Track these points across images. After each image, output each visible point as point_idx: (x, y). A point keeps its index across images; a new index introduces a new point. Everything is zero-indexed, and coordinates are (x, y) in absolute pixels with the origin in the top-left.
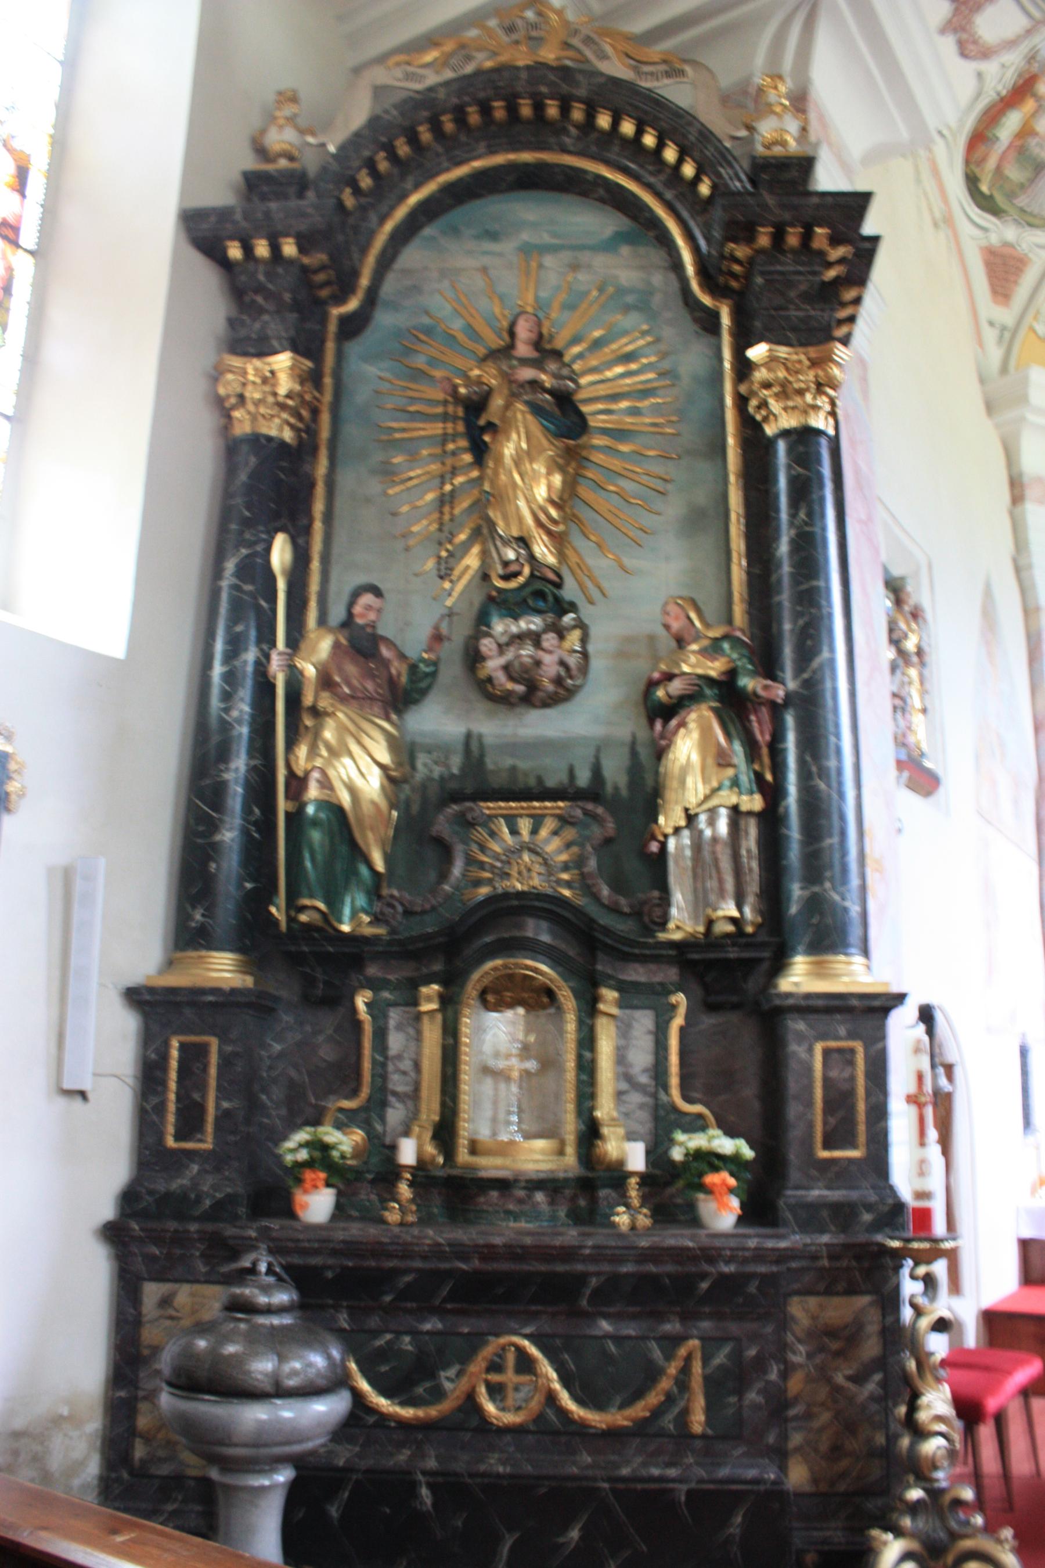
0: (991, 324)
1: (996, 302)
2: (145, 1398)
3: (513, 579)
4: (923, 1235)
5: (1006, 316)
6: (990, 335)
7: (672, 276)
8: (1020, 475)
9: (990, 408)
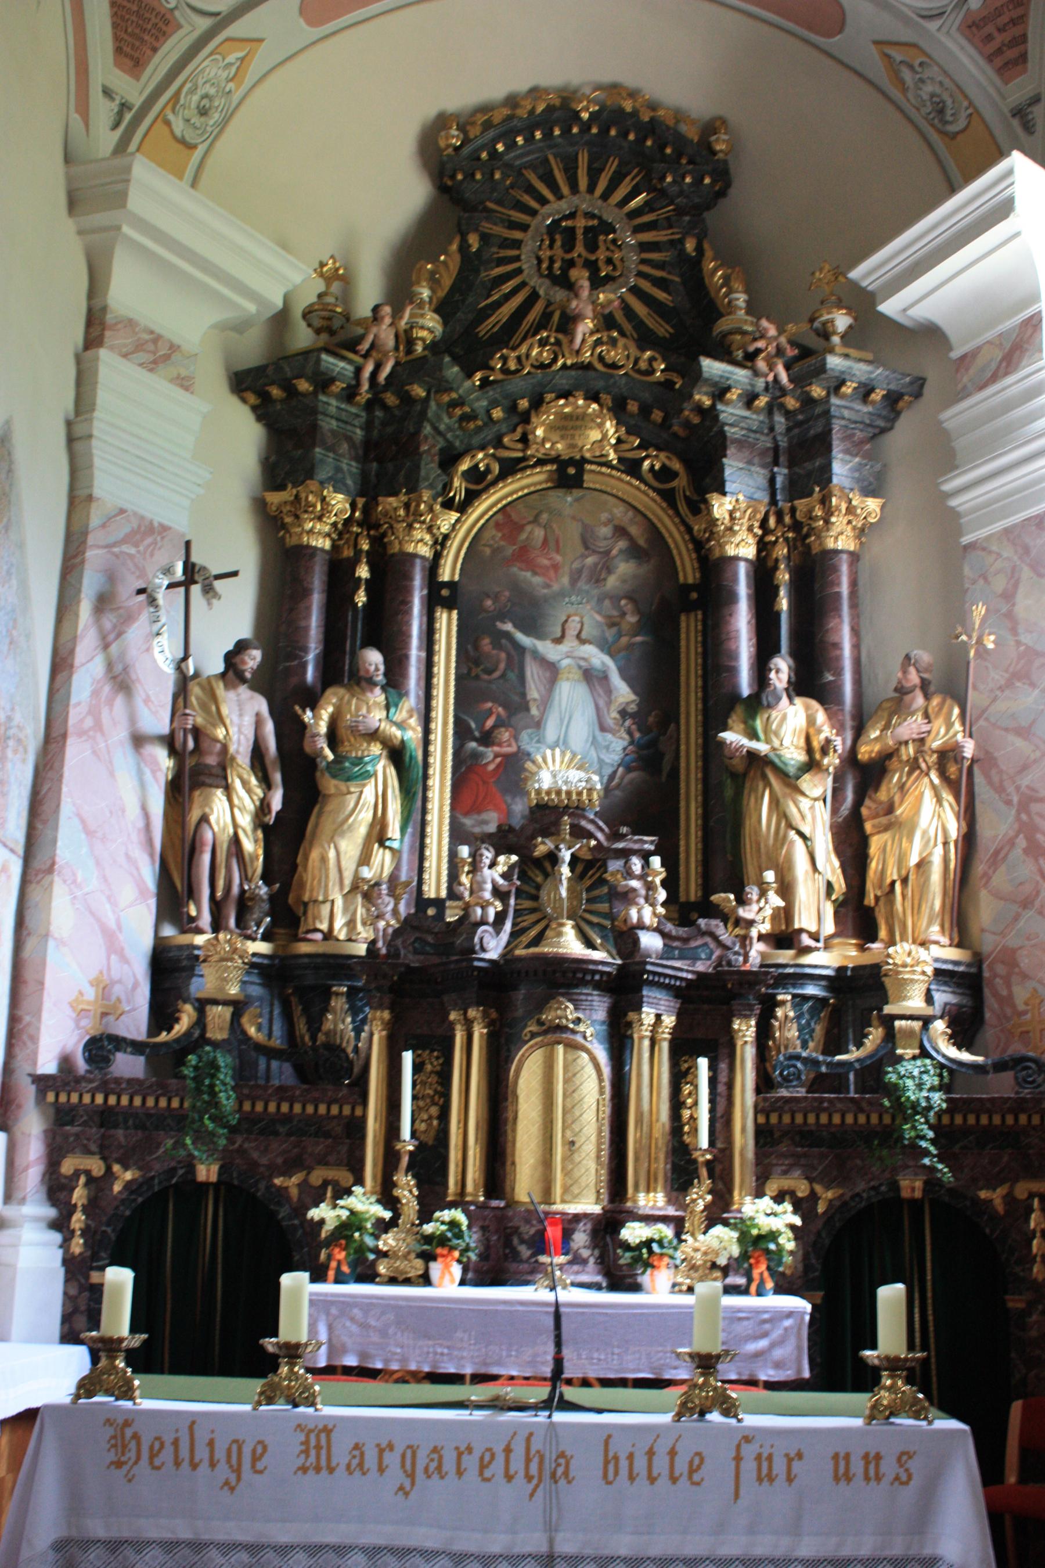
0: (107, 93)
1: (117, 64)
2: (677, 122)
3: (318, 774)
4: (749, 364)
5: (134, 91)
6: (103, 111)
7: (20, 1013)
8: (104, 309)
9: (73, 204)
